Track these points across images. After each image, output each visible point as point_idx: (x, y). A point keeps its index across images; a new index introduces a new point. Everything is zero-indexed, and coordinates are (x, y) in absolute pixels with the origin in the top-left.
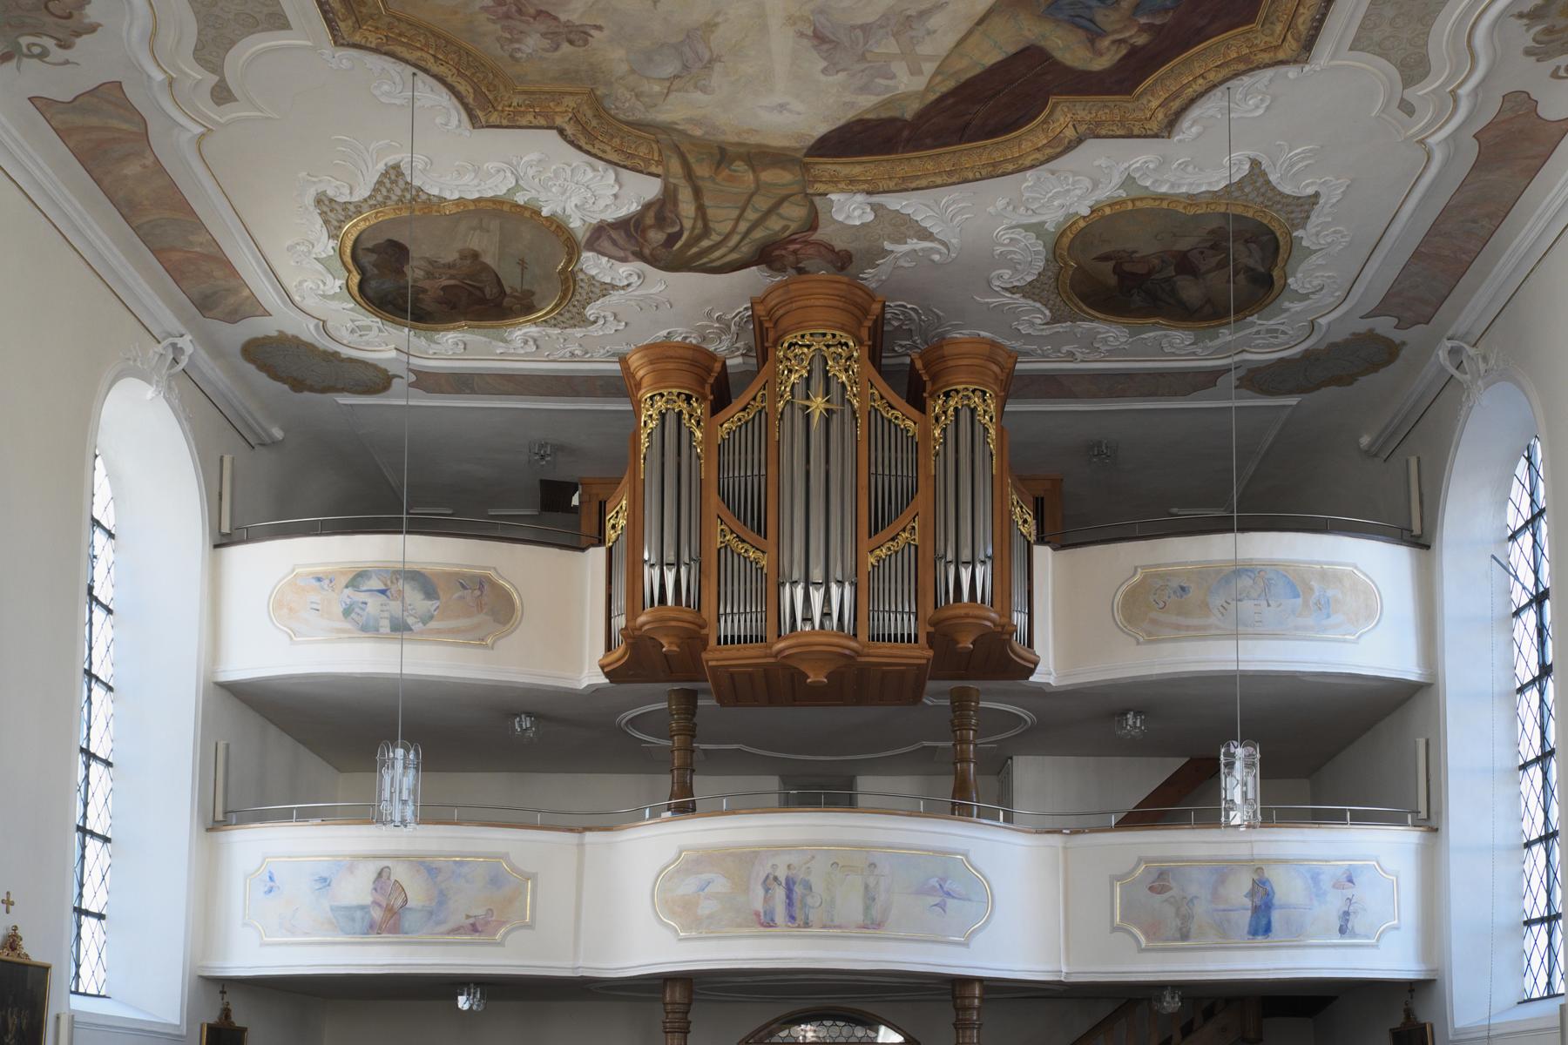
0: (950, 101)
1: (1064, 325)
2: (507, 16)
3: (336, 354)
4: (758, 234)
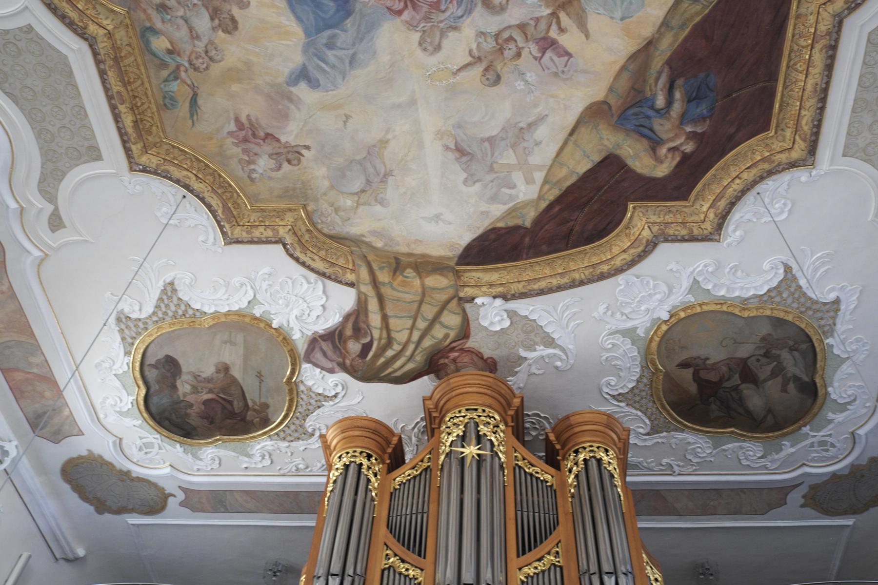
0: (557, 208)
1: (661, 435)
2: (245, 140)
3: (128, 473)
4: (427, 343)
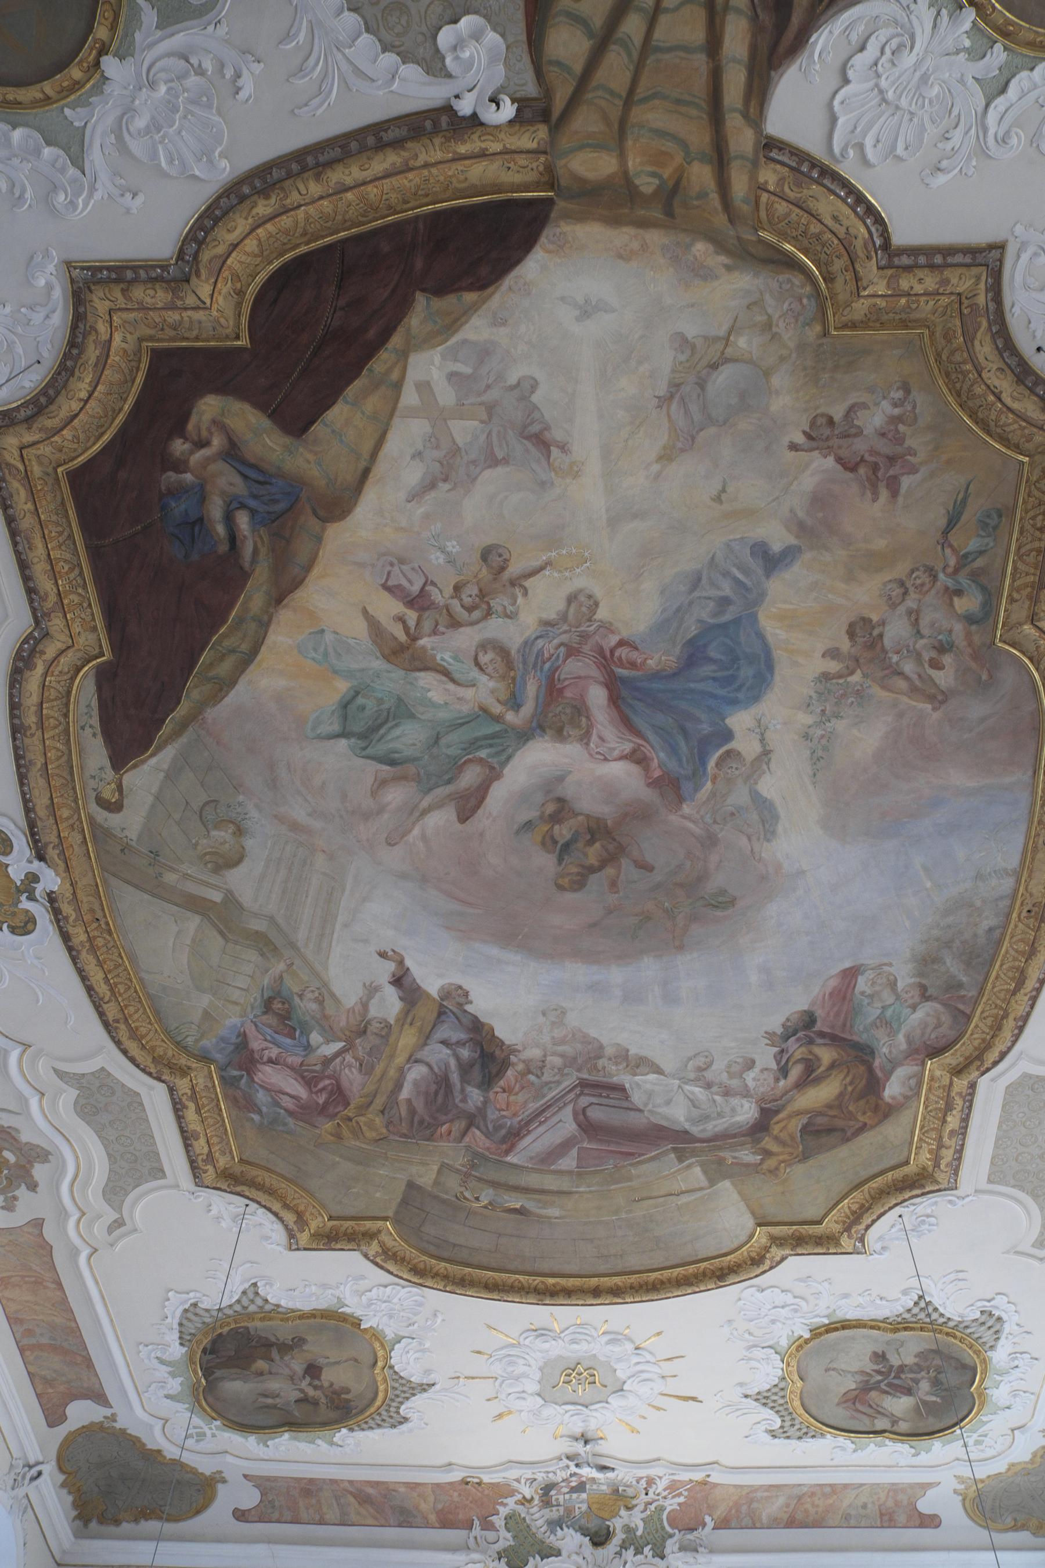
0: (371, 334)
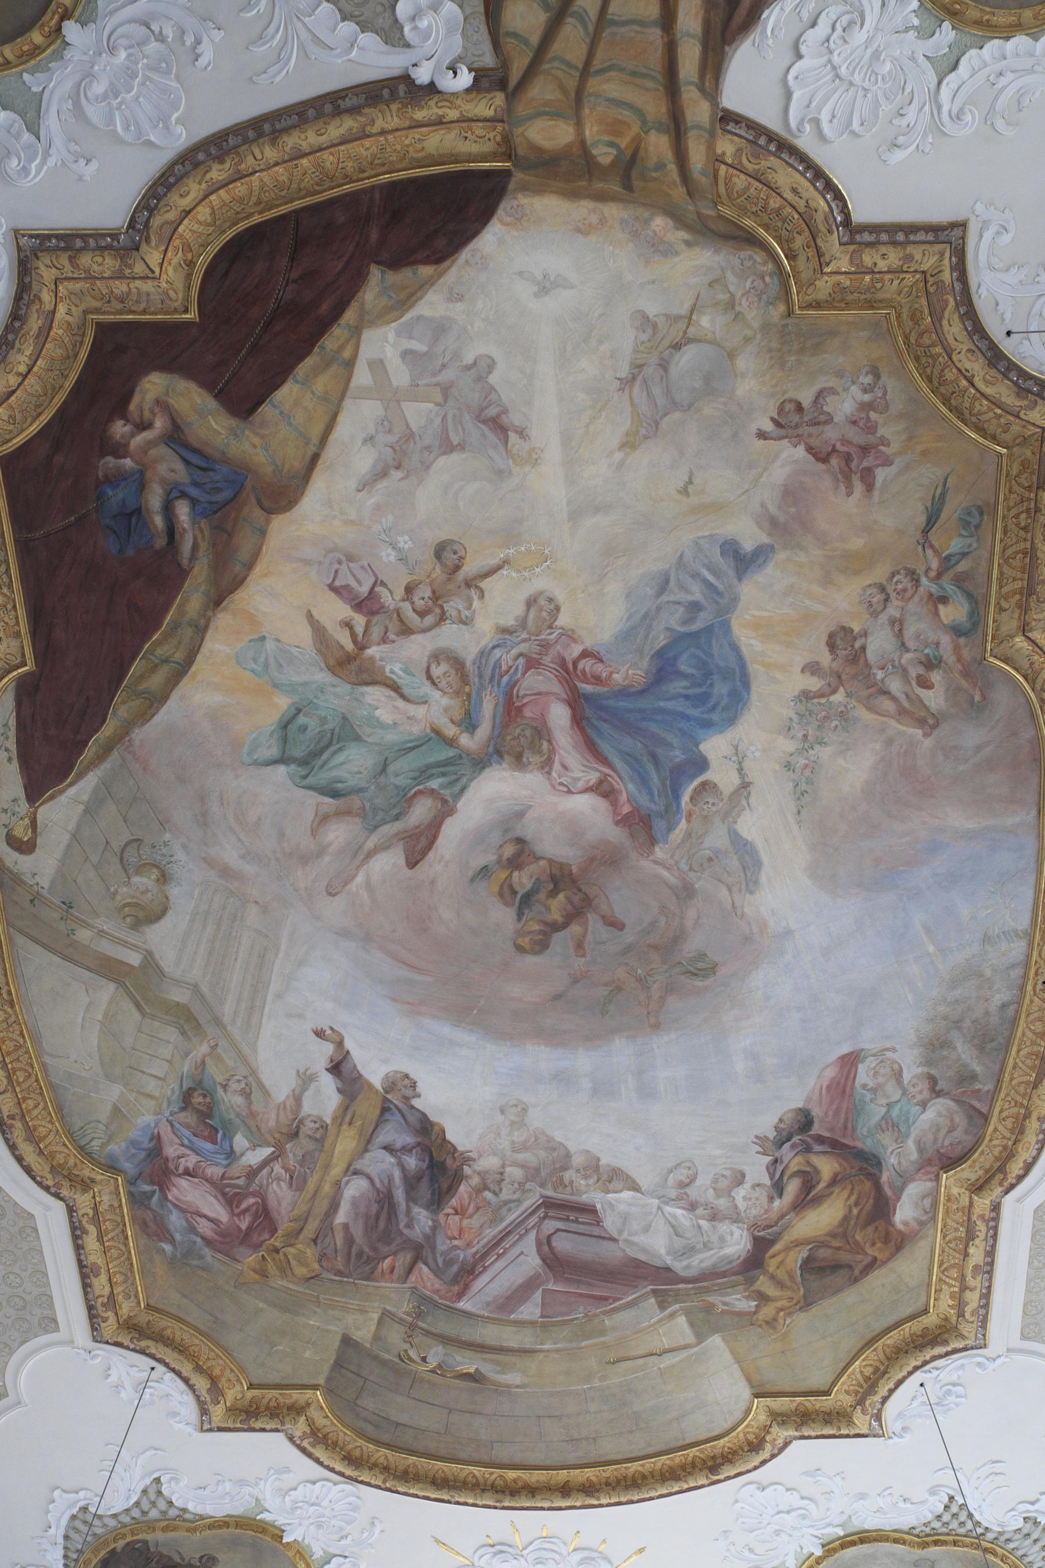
0: (325, 308)
